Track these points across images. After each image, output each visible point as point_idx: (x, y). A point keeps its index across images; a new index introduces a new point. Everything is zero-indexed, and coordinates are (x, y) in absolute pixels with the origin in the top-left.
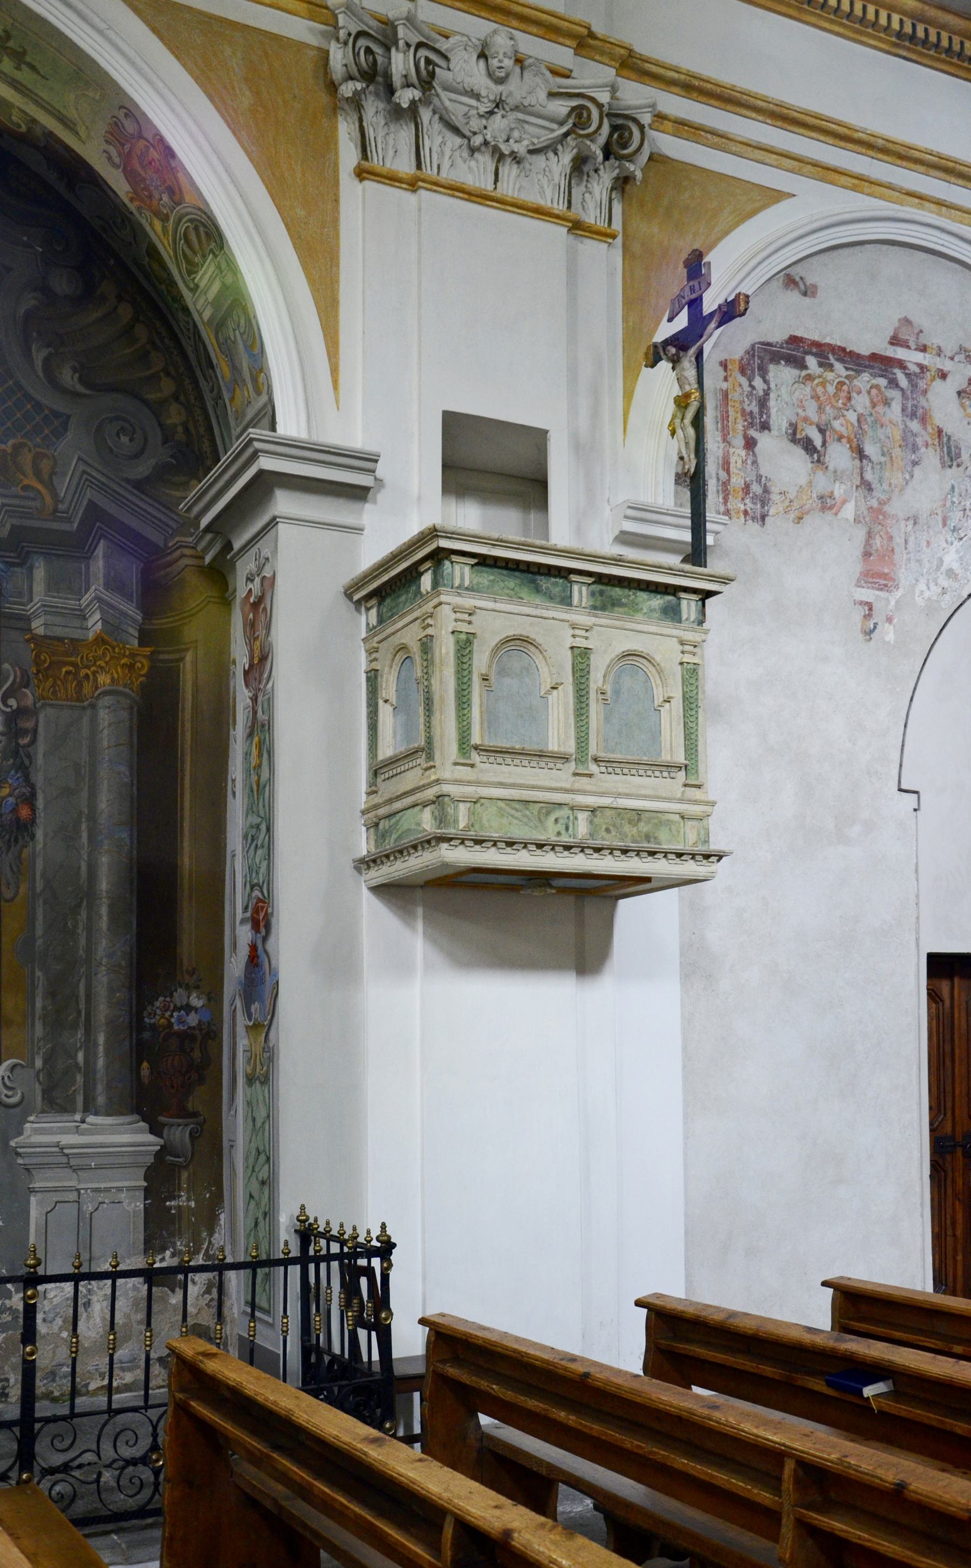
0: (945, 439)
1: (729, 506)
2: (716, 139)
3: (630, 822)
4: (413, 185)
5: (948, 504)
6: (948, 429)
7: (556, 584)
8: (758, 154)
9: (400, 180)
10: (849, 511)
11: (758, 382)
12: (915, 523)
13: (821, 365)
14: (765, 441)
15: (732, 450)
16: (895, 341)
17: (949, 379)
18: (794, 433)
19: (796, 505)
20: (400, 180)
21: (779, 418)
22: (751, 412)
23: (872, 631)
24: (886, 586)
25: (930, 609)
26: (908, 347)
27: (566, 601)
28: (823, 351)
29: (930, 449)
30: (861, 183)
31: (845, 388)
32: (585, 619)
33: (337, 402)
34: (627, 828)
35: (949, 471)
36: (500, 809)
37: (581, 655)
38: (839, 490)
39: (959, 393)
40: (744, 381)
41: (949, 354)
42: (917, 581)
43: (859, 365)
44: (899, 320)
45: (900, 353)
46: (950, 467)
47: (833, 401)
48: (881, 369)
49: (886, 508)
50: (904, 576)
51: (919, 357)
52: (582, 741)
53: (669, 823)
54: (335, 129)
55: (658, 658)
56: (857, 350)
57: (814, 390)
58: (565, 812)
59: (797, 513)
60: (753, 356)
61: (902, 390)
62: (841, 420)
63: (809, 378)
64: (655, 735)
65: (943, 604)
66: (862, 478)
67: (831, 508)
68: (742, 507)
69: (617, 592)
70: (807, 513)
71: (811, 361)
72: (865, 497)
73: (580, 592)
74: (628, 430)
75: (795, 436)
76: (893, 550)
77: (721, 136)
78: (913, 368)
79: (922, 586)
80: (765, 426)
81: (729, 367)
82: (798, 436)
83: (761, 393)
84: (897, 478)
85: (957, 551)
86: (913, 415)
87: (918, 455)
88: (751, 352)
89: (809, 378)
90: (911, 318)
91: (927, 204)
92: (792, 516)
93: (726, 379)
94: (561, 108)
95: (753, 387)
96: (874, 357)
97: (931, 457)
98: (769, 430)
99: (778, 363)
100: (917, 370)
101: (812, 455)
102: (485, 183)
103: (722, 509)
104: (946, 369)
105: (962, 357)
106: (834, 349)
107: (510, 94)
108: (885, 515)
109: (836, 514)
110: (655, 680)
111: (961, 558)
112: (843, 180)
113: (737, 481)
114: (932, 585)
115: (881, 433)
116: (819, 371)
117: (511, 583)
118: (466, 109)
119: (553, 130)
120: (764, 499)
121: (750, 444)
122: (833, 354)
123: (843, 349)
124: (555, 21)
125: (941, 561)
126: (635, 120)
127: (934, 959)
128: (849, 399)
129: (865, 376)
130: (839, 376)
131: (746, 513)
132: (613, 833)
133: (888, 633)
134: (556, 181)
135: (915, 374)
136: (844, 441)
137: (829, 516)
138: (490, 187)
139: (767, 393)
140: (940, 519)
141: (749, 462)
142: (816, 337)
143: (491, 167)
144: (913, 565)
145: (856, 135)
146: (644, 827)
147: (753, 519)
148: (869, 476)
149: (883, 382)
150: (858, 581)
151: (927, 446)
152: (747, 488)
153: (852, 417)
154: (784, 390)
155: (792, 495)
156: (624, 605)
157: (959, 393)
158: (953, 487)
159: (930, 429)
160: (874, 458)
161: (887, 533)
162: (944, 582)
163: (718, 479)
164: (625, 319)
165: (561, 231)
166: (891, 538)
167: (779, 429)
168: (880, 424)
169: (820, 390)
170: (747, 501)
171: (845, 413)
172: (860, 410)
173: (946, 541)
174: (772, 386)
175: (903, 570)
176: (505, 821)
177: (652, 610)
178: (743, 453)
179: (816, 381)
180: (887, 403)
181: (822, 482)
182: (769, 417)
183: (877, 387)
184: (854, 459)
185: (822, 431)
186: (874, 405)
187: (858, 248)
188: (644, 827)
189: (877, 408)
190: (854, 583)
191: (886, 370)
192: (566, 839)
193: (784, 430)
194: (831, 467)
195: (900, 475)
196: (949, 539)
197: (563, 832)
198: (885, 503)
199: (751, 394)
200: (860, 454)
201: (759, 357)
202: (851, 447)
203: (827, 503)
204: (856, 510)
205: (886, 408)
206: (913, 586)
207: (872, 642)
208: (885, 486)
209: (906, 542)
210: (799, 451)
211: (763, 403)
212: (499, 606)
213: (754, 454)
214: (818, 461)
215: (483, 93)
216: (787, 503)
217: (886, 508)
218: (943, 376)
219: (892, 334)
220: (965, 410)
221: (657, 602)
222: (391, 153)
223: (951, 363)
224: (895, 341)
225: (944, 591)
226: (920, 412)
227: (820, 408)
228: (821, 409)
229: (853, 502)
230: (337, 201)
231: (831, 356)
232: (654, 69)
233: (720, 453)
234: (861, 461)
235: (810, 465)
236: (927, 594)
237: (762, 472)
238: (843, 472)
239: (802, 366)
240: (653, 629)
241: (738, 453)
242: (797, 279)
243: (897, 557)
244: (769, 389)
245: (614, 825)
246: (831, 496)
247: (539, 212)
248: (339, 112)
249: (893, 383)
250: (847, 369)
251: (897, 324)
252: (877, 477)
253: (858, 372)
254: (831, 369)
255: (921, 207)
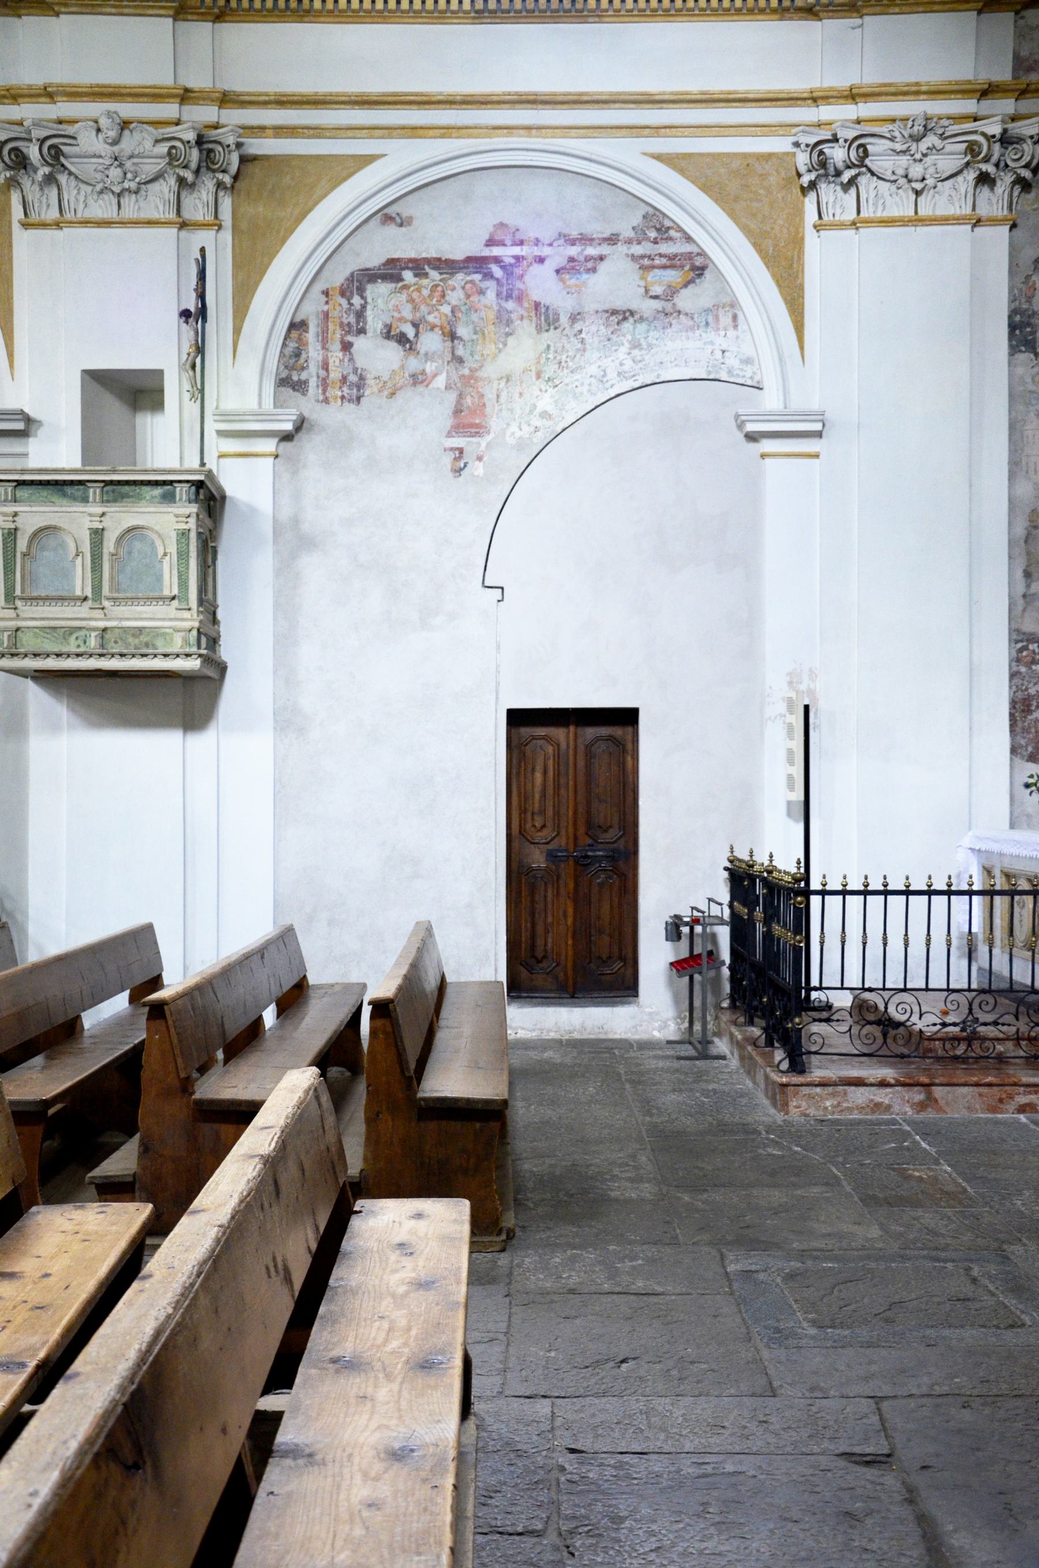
0: (543, 310)
1: (328, 394)
2: (312, 132)
3: (134, 635)
4: (57, 225)
5: (543, 361)
6: (546, 300)
7: (79, 490)
8: (350, 133)
9: (50, 225)
10: (440, 381)
11: (357, 301)
12: (508, 381)
13: (416, 275)
14: (360, 344)
15: (330, 354)
16: (491, 242)
17: (547, 262)
18: (389, 332)
19: (389, 384)
20: (50, 225)
21: (374, 322)
22: (349, 323)
23: (461, 469)
24: (477, 433)
25: (520, 446)
26: (504, 245)
27: (85, 500)
28: (418, 266)
29: (526, 322)
30: (447, 131)
31: (439, 289)
32: (99, 510)
33: (12, 375)
34: (131, 640)
35: (546, 334)
36: (35, 633)
37: (97, 535)
38: (430, 367)
39: (558, 271)
40: (344, 302)
41: (547, 242)
42: (508, 425)
43: (453, 268)
44: (494, 226)
45: (496, 251)
46: (547, 331)
47: (428, 301)
48: (475, 268)
49: (478, 374)
50: (495, 424)
51: (517, 251)
52: (97, 588)
53: (164, 634)
54: (9, 200)
55: (157, 528)
56: (451, 257)
57: (410, 295)
58: (82, 633)
59: (390, 390)
60: (353, 281)
61: (497, 280)
62: (436, 313)
63: (406, 287)
64: (159, 578)
65: (535, 440)
66: (453, 353)
67: (422, 382)
68: (340, 394)
69: (127, 488)
70: (401, 388)
71: (408, 276)
72: (456, 369)
73: (94, 492)
74: (237, 353)
75: (388, 334)
76: (484, 405)
77: (316, 128)
78: (509, 260)
79: (514, 428)
80: (362, 331)
81: (331, 293)
82: (392, 333)
83: (358, 307)
84: (490, 348)
85: (552, 397)
86: (509, 297)
87: (512, 327)
88: (351, 278)
89: (406, 287)
90: (505, 222)
91: (515, 131)
92: (386, 393)
93: (327, 303)
94: (163, 148)
95: (351, 305)
96: (469, 260)
97: (525, 329)
98: (365, 333)
99: (375, 282)
100: (513, 261)
101: (404, 346)
102: (111, 213)
103: (321, 398)
104: (543, 254)
105: (562, 241)
106: (428, 261)
107: (122, 151)
108: (476, 380)
109: (427, 386)
110: (158, 543)
111: (556, 402)
112: (431, 132)
113: (335, 375)
114: (525, 427)
115: (474, 317)
116: (413, 280)
117: (45, 493)
118: (95, 166)
119: (159, 164)
120: (360, 384)
121: (347, 347)
122: (429, 265)
123: (439, 259)
124: (157, 91)
125: (535, 406)
126: (220, 143)
127: (517, 718)
128: (443, 296)
129: (460, 276)
130: (433, 281)
131: (343, 397)
132: (120, 643)
133: (478, 469)
134: (167, 198)
135: (511, 265)
136: (437, 330)
137: (420, 388)
138: (115, 215)
139: (364, 307)
140: (533, 374)
141: (346, 360)
142: (413, 255)
143: (115, 201)
144: (505, 413)
145: (434, 99)
146: (144, 639)
147: (349, 401)
148: (460, 352)
149: (477, 277)
150: (449, 432)
151: (522, 318)
152: (344, 379)
153: (446, 309)
154: (380, 301)
155: (385, 378)
156: (132, 497)
157: (558, 271)
158: (548, 347)
159: (526, 305)
160: (466, 337)
161: (478, 392)
162: (537, 422)
163: (318, 377)
164: (235, 276)
165: (173, 231)
166: (482, 396)
167: (375, 331)
168: (473, 309)
169: (415, 295)
170: (345, 389)
171: (440, 307)
172: (454, 302)
173: (541, 390)
174: (369, 300)
175: (494, 419)
176: (39, 641)
177: (153, 497)
178: (340, 355)
179: (412, 289)
180: (482, 292)
181: (414, 364)
182: (365, 323)
183: (472, 282)
184: (444, 341)
185: (416, 325)
186: (468, 296)
187: (452, 179)
188: (144, 639)
189: (471, 299)
190: (444, 434)
191: (480, 267)
192: (82, 650)
193: (379, 331)
194: (422, 352)
195: (493, 346)
196: (544, 389)
197: (82, 644)
198: (477, 370)
199: (349, 309)
200: (453, 336)
201: (358, 281)
202: (443, 333)
203: (418, 379)
204: (447, 380)
205: (482, 298)
206: (504, 430)
207: (461, 478)
208: (477, 357)
209: (498, 396)
210: (393, 344)
211: (360, 315)
212: (34, 509)
213: (350, 354)
214: (410, 349)
215: (103, 154)
216: (381, 384)
217: (478, 374)
218: (541, 260)
219: (487, 238)
220: (564, 283)
221: (158, 491)
222: (45, 207)
223: (550, 248)
224: (491, 242)
225: (537, 429)
226: (516, 293)
227: (415, 308)
228: (415, 309)
229: (444, 375)
230: (11, 246)
231: (426, 267)
232: (247, 98)
233: (320, 358)
234: (452, 341)
235: (402, 353)
236: (518, 434)
237: (359, 365)
238: (434, 353)
239: (399, 279)
240: (152, 509)
241: (336, 355)
242: (394, 215)
243: (488, 410)
244: (366, 302)
245: (121, 639)
246: (423, 372)
247: (150, 223)
248: (12, 189)
249: (488, 276)
250: (441, 274)
251: (491, 229)
252: (468, 352)
253: (452, 274)
254: (426, 275)
255: (510, 135)
